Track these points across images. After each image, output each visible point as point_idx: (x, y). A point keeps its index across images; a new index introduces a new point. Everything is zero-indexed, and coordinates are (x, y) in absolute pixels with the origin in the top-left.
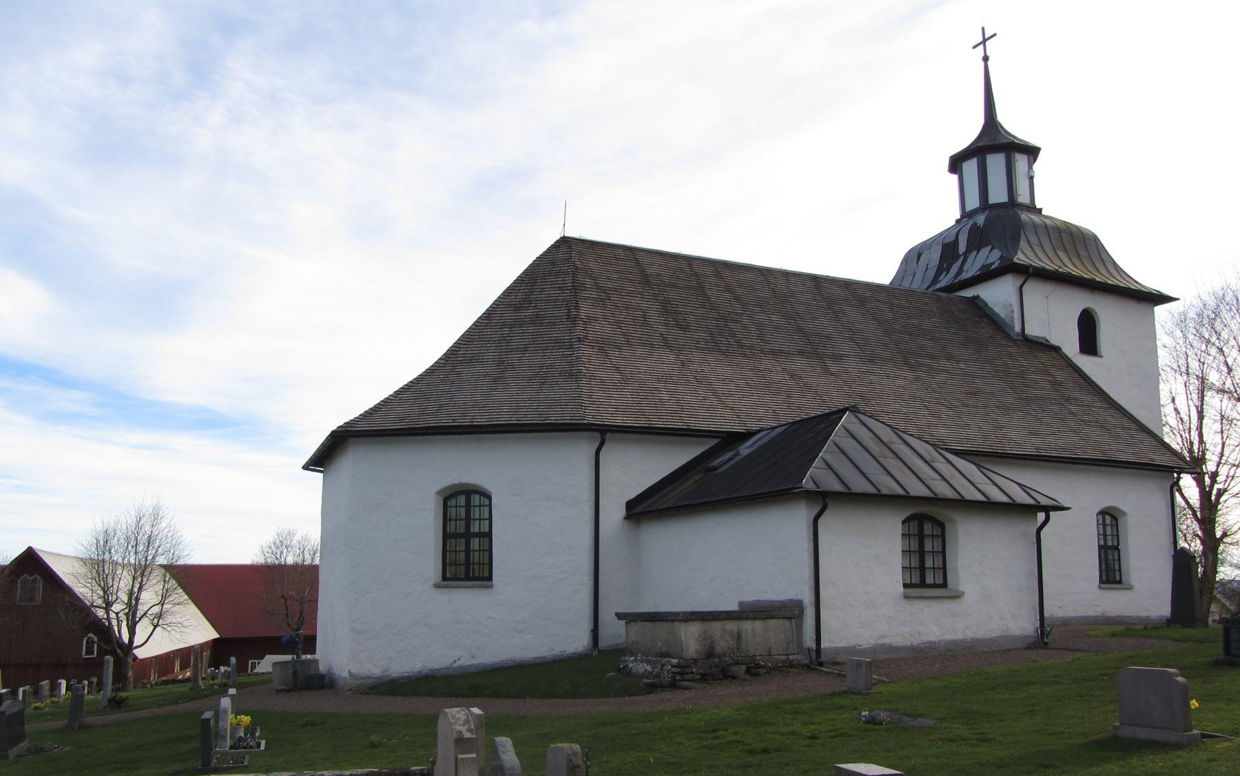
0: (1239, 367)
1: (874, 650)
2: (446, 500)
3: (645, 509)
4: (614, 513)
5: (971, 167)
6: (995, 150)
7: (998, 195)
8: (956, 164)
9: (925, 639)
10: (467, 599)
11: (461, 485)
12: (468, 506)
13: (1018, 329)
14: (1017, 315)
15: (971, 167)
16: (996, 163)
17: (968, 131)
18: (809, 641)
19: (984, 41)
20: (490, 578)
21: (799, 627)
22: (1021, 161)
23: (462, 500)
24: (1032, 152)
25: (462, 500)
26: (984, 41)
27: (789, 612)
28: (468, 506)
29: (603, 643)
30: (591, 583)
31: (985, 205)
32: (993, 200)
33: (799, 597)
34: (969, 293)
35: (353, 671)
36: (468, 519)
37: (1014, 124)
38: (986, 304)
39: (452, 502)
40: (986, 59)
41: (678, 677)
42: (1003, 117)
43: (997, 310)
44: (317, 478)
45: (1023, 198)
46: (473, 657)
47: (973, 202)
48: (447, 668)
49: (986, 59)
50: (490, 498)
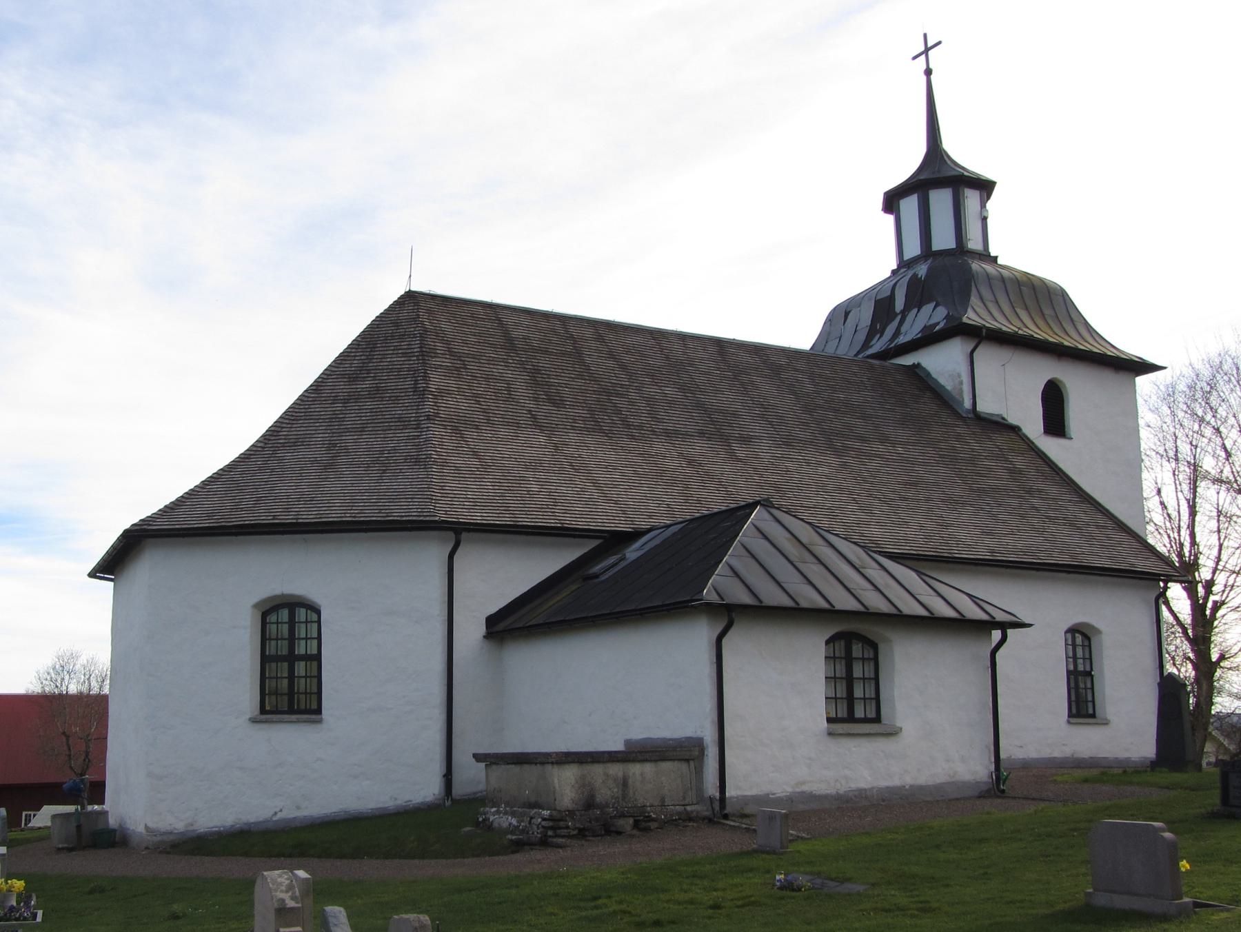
1: (790, 799)
3: (505, 627)
4: (471, 631)
5: (910, 206)
6: (939, 184)
7: (943, 239)
8: (892, 201)
9: (399, 802)
10: (290, 738)
11: (283, 596)
12: (292, 622)
13: (967, 404)
14: (966, 388)
15: (910, 206)
16: (941, 200)
17: (907, 161)
18: (711, 789)
19: (927, 50)
21: (699, 771)
22: (971, 198)
23: (284, 614)
24: (985, 187)
25: (284, 614)
26: (927, 50)
27: (685, 752)
28: (292, 622)
29: (457, 791)
30: (443, 717)
32: (937, 245)
33: (699, 734)
34: (907, 360)
35: (150, 825)
36: (292, 639)
37: (965, 152)
38: (928, 374)
39: (273, 618)
40: (928, 72)
41: (550, 833)
42: (953, 146)
43: (942, 381)
44: (105, 588)
45: (974, 244)
46: (298, 808)
47: (913, 249)
48: (266, 821)
49: (928, 72)
50: (318, 612)
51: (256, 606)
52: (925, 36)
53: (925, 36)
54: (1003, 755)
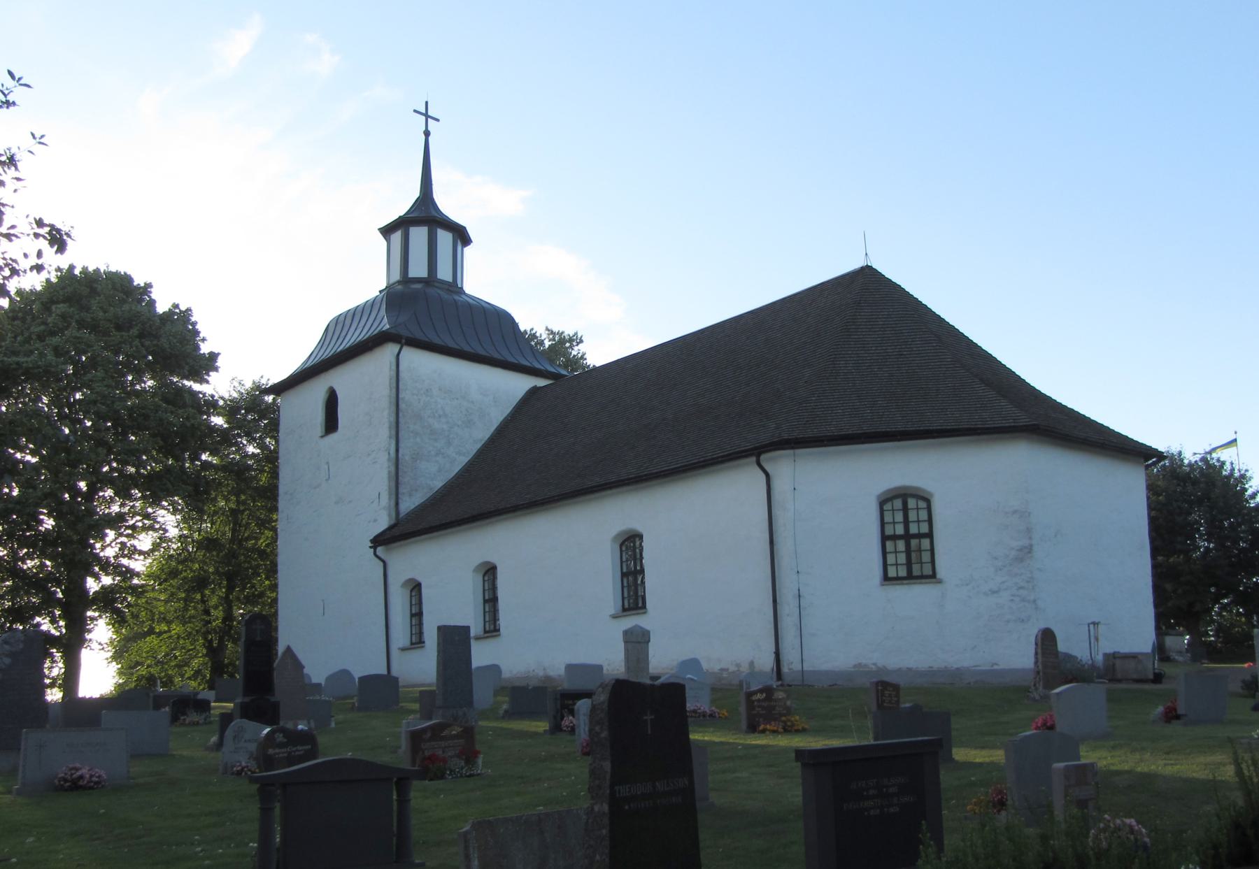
0: (2, 516)
2: (882, 504)
7: (418, 269)
8: (387, 231)
10: (912, 598)
11: (924, 491)
12: (905, 509)
16: (419, 235)
17: (402, 204)
20: (644, 606)
23: (898, 503)
24: (461, 236)
28: (905, 509)
30: (772, 619)
31: (406, 280)
36: (906, 522)
37: (448, 204)
39: (887, 507)
45: (444, 273)
47: (396, 276)
50: (928, 501)
51: (615, 538)
52: (437, 120)
53: (437, 120)
54: (785, 669)
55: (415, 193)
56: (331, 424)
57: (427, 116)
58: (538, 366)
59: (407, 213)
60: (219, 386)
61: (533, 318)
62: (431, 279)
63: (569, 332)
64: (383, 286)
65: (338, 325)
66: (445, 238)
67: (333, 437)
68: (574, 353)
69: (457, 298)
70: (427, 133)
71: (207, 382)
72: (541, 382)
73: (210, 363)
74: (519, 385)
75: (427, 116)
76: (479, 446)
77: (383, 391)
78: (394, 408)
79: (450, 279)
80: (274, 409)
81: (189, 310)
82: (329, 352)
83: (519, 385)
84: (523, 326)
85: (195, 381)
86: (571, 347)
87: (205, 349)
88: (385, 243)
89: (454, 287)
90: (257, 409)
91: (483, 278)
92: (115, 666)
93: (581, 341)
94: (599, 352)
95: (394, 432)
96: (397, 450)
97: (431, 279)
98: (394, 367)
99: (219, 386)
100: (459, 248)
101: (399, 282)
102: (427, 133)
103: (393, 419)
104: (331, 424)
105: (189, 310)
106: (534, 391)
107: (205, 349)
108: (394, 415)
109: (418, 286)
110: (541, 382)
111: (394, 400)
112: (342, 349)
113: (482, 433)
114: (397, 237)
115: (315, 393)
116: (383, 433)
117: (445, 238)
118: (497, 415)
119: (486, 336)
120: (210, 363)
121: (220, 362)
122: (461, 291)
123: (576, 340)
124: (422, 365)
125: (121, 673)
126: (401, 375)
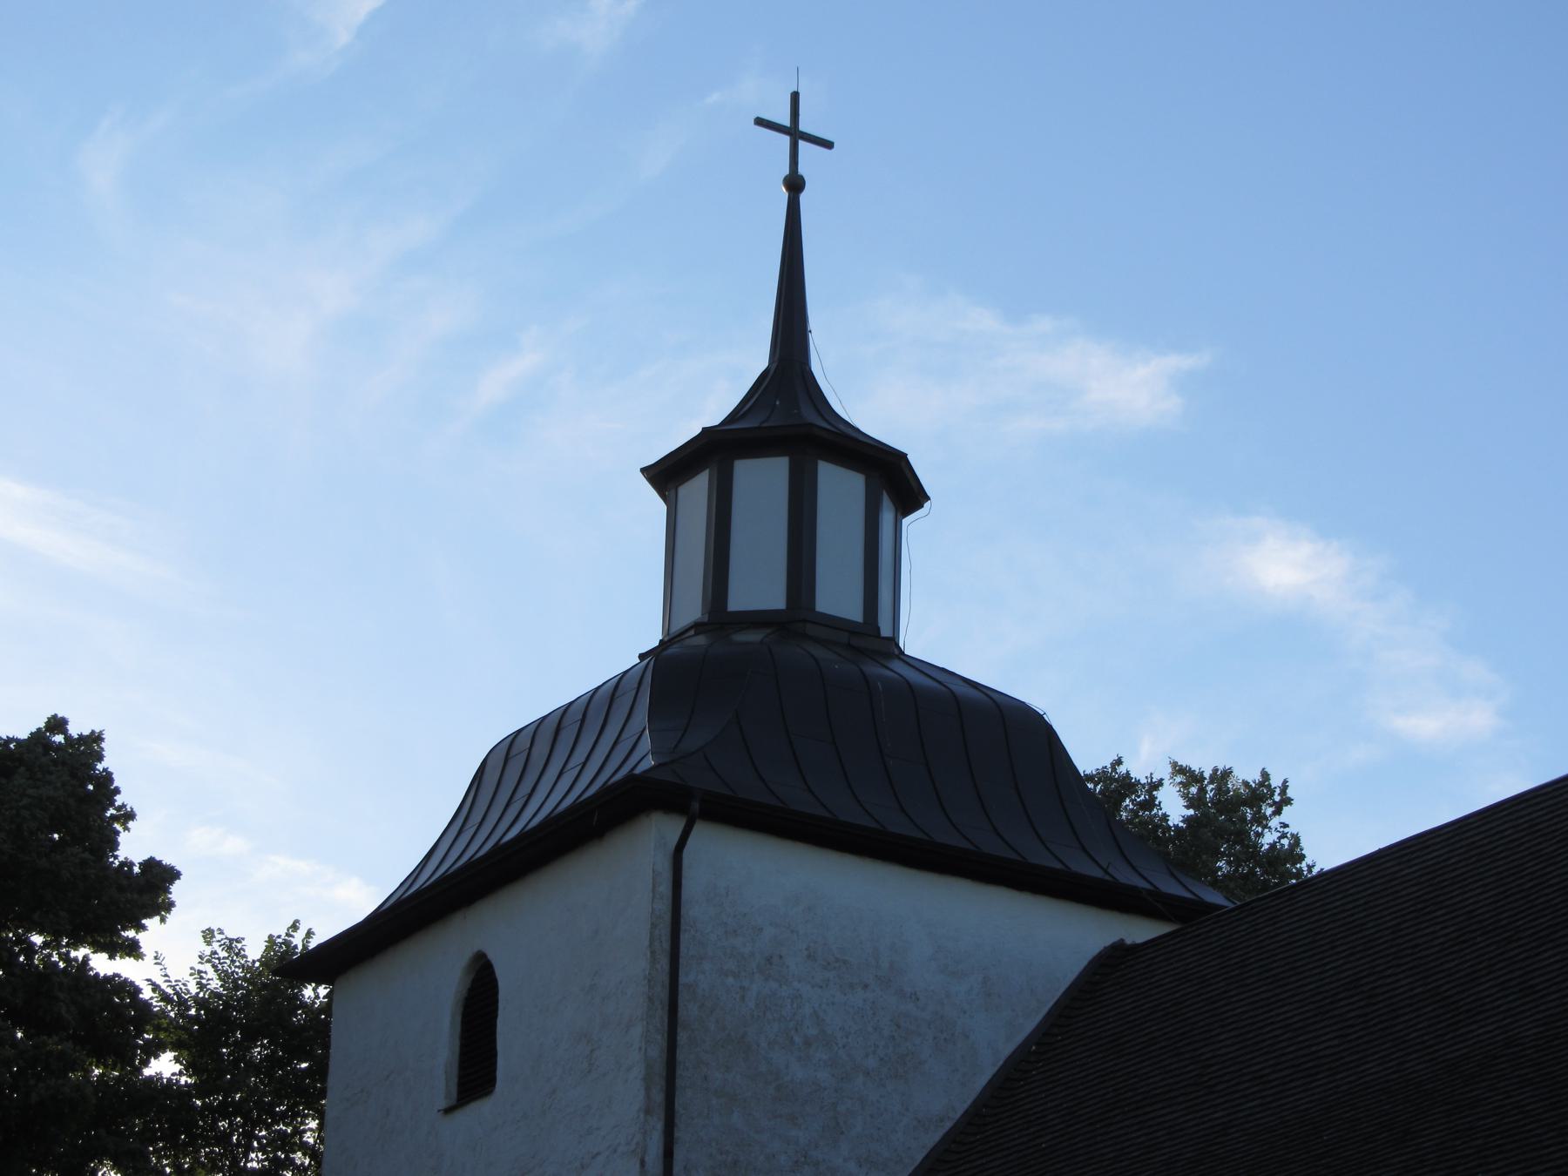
7: (759, 586)
8: (666, 475)
16: (762, 483)
24: (893, 482)
31: (719, 617)
37: (865, 390)
45: (838, 596)
47: (692, 610)
55: (752, 358)
56: (476, 1072)
57: (794, 133)
58: (1126, 877)
59: (724, 423)
60: (166, 959)
61: (1128, 728)
62: (798, 617)
63: (1246, 773)
64: (652, 637)
65: (510, 763)
66: (841, 491)
67: (482, 1109)
68: (1268, 838)
69: (872, 669)
70: (795, 184)
71: (133, 950)
72: (1139, 931)
73: (152, 888)
74: (1067, 938)
75: (794, 133)
76: (932, 1138)
77: (632, 964)
78: (661, 1014)
79: (853, 611)
80: (319, 1024)
81: (96, 738)
82: (480, 846)
83: (1067, 938)
84: (1087, 757)
85: (98, 948)
86: (1261, 820)
87: (133, 847)
88: (662, 507)
89: (872, 639)
90: (272, 1017)
91: (960, 611)
92: (173, 897)
93: (1287, 801)
94: (1331, 833)
95: (659, 1097)
96: (668, 1154)
97: (798, 617)
98: (665, 888)
99: (166, 959)
100: (887, 516)
101: (697, 627)
102: (795, 184)
103: (657, 1052)
104: (476, 1072)
105: (96, 738)
106: (1114, 958)
107: (133, 847)
108: (661, 1040)
109: (753, 637)
110: (1139, 931)
111: (663, 994)
112: (529, 826)
113: (946, 1094)
114: (697, 490)
115: (434, 970)
116: (626, 1097)
117: (841, 491)
118: (995, 1039)
119: (975, 784)
120: (152, 888)
121: (177, 891)
122: (890, 648)
123: (1264, 796)
124: (756, 880)
125: (97, 974)
126: (690, 912)
